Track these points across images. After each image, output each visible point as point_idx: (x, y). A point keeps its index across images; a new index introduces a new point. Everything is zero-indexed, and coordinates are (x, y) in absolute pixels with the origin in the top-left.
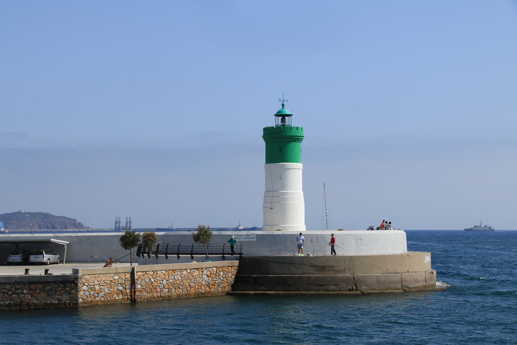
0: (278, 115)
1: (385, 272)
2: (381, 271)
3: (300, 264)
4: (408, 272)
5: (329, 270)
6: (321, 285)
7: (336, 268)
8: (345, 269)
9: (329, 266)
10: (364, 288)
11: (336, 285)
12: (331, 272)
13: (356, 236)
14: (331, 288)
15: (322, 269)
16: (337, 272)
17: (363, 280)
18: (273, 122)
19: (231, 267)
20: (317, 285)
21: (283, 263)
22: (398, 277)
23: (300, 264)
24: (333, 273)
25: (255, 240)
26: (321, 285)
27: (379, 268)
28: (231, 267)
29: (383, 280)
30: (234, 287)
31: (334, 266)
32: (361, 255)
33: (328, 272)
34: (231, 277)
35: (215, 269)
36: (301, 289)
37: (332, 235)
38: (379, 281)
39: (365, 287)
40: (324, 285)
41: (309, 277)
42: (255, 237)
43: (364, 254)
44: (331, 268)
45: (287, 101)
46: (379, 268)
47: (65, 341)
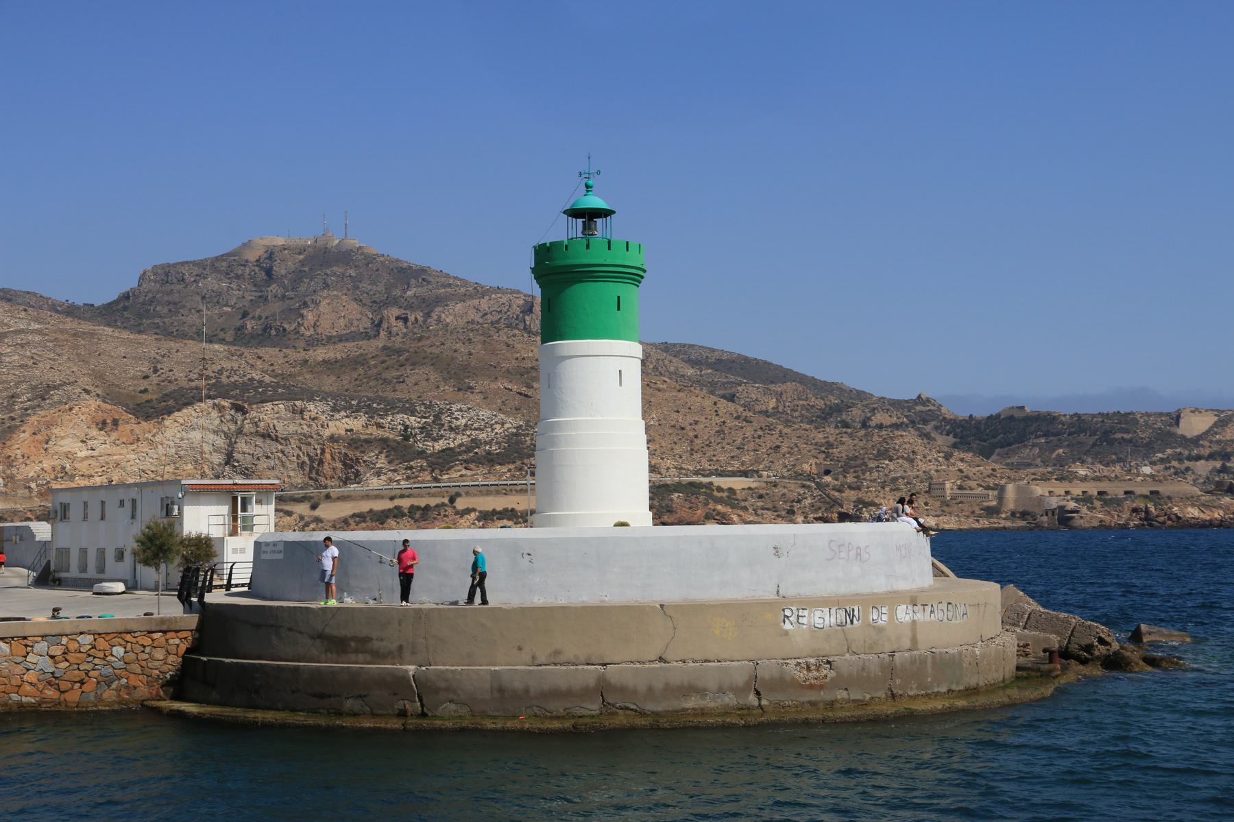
0: (575, 213)
1: (542, 659)
2: (528, 658)
3: (290, 629)
4: (661, 659)
5: (357, 651)
6: (322, 696)
7: (376, 645)
8: (400, 648)
9: (355, 639)
10: (447, 714)
11: (360, 696)
12: (361, 657)
13: (514, 545)
14: (349, 704)
15: (339, 645)
16: (378, 656)
17: (443, 685)
18: (560, 230)
19: (165, 632)
20: (314, 695)
21: (259, 626)
22: (739, 672)
23: (290, 629)
24: (369, 658)
25: (280, 556)
26: (322, 696)
27: (520, 649)
28: (165, 632)
29: (517, 685)
30: (178, 686)
31: (371, 639)
32: (527, 604)
33: (353, 657)
34: (166, 658)
35: (88, 639)
36: (280, 706)
37: (406, 541)
38: (501, 690)
39: (453, 707)
40: (330, 696)
41: (297, 669)
42: (281, 547)
43: (538, 600)
44: (362, 645)
45: (598, 173)
46: (520, 649)
47: (1030, 726)
